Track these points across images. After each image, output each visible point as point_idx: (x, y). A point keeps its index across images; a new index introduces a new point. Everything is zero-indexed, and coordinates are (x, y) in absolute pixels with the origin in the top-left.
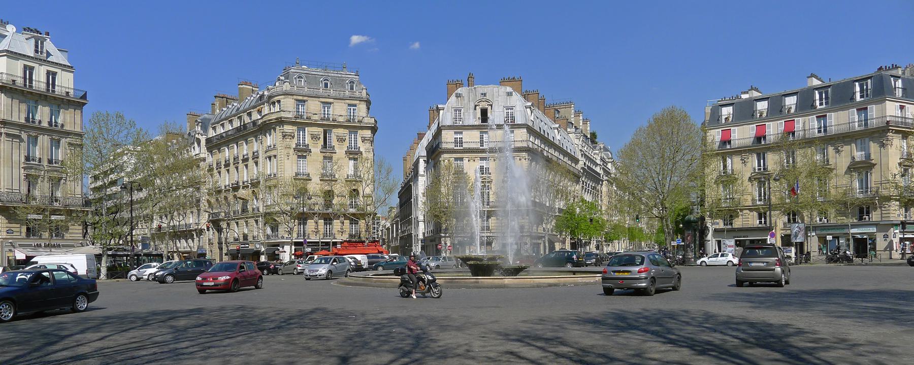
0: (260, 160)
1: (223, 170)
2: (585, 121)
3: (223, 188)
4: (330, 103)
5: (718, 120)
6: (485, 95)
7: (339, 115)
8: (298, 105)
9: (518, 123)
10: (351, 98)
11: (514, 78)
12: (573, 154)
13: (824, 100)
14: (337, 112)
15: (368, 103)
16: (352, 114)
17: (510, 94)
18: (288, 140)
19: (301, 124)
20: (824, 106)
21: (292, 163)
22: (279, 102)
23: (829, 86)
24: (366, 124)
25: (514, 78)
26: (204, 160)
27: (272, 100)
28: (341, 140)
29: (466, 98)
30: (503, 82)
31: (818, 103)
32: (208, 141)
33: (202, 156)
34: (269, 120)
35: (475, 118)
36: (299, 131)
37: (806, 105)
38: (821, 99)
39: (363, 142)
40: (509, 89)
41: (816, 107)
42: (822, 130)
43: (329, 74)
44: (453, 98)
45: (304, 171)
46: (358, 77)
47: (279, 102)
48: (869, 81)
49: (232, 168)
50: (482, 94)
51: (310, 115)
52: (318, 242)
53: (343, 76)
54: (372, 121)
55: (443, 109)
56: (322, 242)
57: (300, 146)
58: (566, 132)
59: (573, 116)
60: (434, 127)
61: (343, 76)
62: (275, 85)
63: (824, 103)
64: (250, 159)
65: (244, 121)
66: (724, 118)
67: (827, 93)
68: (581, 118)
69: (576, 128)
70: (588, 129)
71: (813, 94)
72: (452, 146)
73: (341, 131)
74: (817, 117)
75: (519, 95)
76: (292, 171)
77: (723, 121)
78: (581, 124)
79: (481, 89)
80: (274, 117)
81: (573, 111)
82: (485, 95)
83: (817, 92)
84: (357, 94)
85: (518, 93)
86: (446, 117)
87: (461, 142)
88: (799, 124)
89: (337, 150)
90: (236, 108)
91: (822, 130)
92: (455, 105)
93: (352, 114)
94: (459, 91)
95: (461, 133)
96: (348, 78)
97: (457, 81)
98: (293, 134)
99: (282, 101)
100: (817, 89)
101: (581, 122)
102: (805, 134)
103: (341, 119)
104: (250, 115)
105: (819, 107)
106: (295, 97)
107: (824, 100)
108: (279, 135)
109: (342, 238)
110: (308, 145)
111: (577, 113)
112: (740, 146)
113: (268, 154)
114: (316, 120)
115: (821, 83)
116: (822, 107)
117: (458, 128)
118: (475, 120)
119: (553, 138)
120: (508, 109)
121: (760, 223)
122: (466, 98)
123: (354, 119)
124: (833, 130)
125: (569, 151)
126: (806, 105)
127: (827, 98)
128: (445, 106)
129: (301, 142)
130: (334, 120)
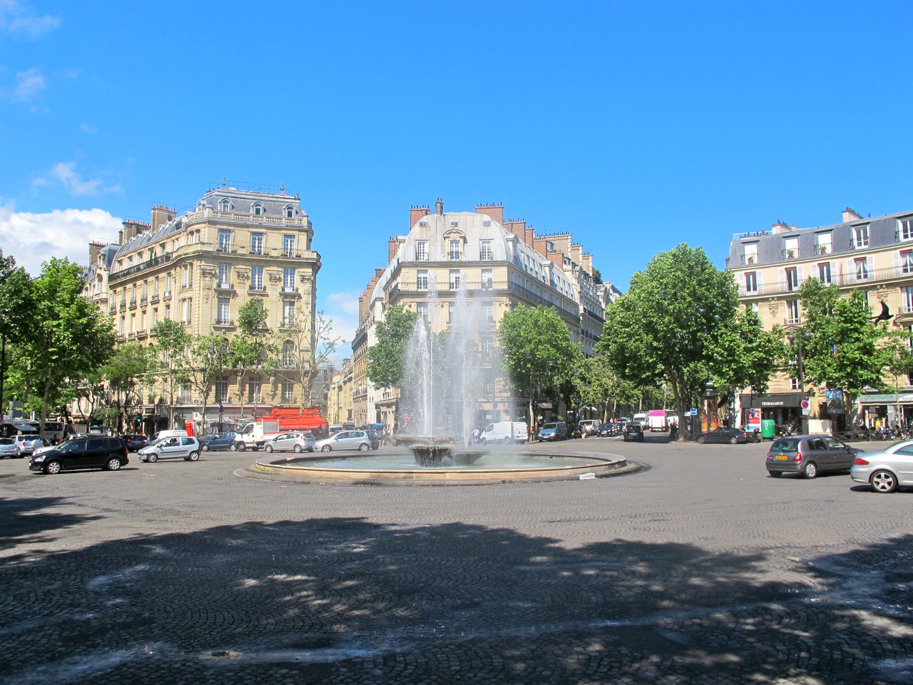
0: (172, 303)
1: (128, 314)
2: (586, 255)
3: (127, 336)
4: (262, 234)
5: (896, 237)
6: (456, 224)
7: (273, 247)
8: (222, 236)
9: (498, 259)
10: (288, 228)
11: (493, 204)
12: (569, 297)
13: (909, 231)
14: (270, 245)
15: (309, 232)
16: (289, 247)
17: (487, 224)
18: (208, 279)
19: (289, 264)
20: (910, 239)
21: (212, 308)
22: (198, 231)
23: (868, 223)
24: (307, 259)
25: (493, 204)
26: (105, 301)
27: (189, 229)
28: (274, 279)
29: (433, 229)
30: (479, 208)
31: (901, 234)
32: (112, 278)
33: (104, 296)
34: (185, 254)
35: (444, 252)
36: (286, 274)
37: (842, 246)
38: (859, 238)
39: (302, 281)
40: (486, 218)
41: (853, 248)
42: (862, 275)
43: (263, 198)
44: (416, 228)
45: (226, 318)
46: (298, 201)
47: (198, 231)
48: (868, 227)
49: (138, 312)
50: (453, 224)
51: (236, 248)
52: (240, 408)
53: (280, 200)
54: (315, 256)
55: (404, 241)
56: (244, 408)
57: (255, 288)
58: (561, 270)
59: (569, 250)
60: (394, 263)
61: (280, 200)
62: (195, 211)
63: (863, 244)
64: (162, 302)
65: (155, 254)
66: (747, 258)
67: (865, 232)
68: (581, 252)
69: (574, 265)
70: (591, 265)
71: (850, 233)
72: (413, 288)
73: (274, 269)
74: (856, 260)
75: (499, 225)
76: (211, 318)
77: (747, 262)
78: (581, 259)
79: (451, 217)
80: (191, 250)
81: (570, 244)
82: (456, 224)
83: (899, 221)
84: (296, 223)
85: (498, 222)
86: (405, 252)
87: (426, 283)
88: (836, 266)
89: (269, 291)
90: (148, 238)
91: (862, 275)
92: (418, 237)
93: (289, 247)
94: (424, 219)
95: (426, 271)
96: (284, 202)
97: (423, 207)
98: (213, 272)
99: (202, 230)
100: (853, 226)
101: (581, 256)
102: (842, 281)
103: (274, 254)
104: (163, 246)
105: (857, 248)
106: (218, 226)
107: (909, 231)
108: (197, 272)
109: (272, 403)
110: (265, 287)
111: (575, 246)
112: (766, 292)
113: (183, 296)
114: (243, 255)
115: (856, 219)
116: (906, 240)
117: (419, 265)
118: (443, 255)
119: (544, 277)
120: (485, 243)
121: (794, 387)
122: (433, 229)
123: (291, 254)
124: (874, 276)
125: (564, 294)
126: (842, 246)
127: (865, 237)
128: (406, 238)
129: (257, 283)
130: (266, 255)
